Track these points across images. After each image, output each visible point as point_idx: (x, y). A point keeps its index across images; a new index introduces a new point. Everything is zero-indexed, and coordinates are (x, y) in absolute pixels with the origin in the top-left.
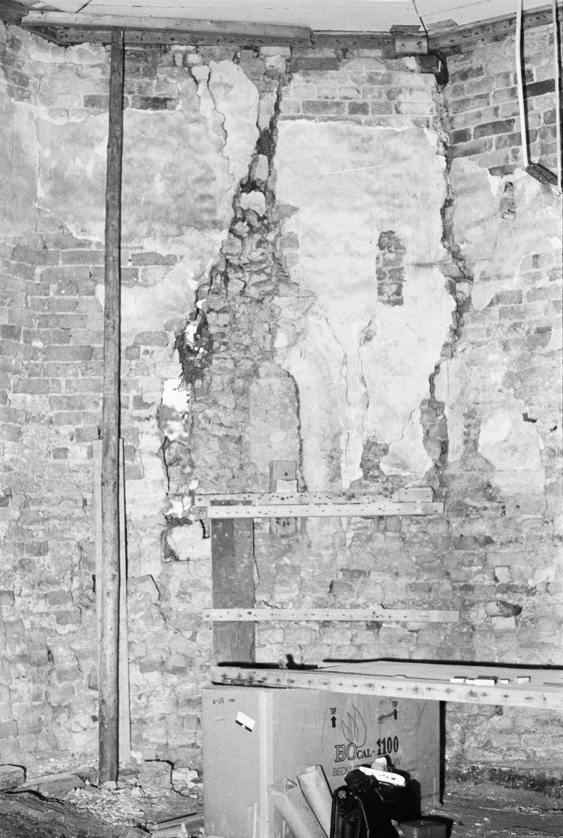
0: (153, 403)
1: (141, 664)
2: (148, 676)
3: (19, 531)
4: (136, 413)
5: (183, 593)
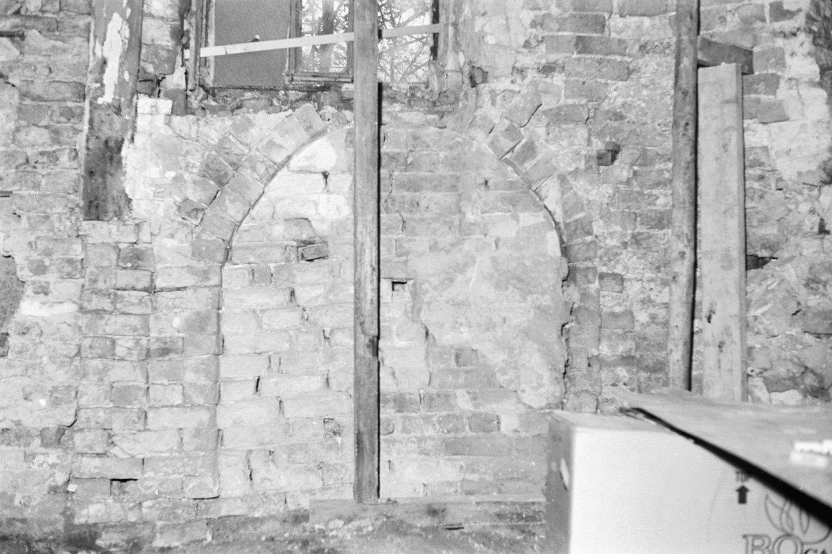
0: (799, 10)
1: (765, 379)
2: (778, 397)
3: (628, 197)
4: (777, 26)
5: (813, 281)
